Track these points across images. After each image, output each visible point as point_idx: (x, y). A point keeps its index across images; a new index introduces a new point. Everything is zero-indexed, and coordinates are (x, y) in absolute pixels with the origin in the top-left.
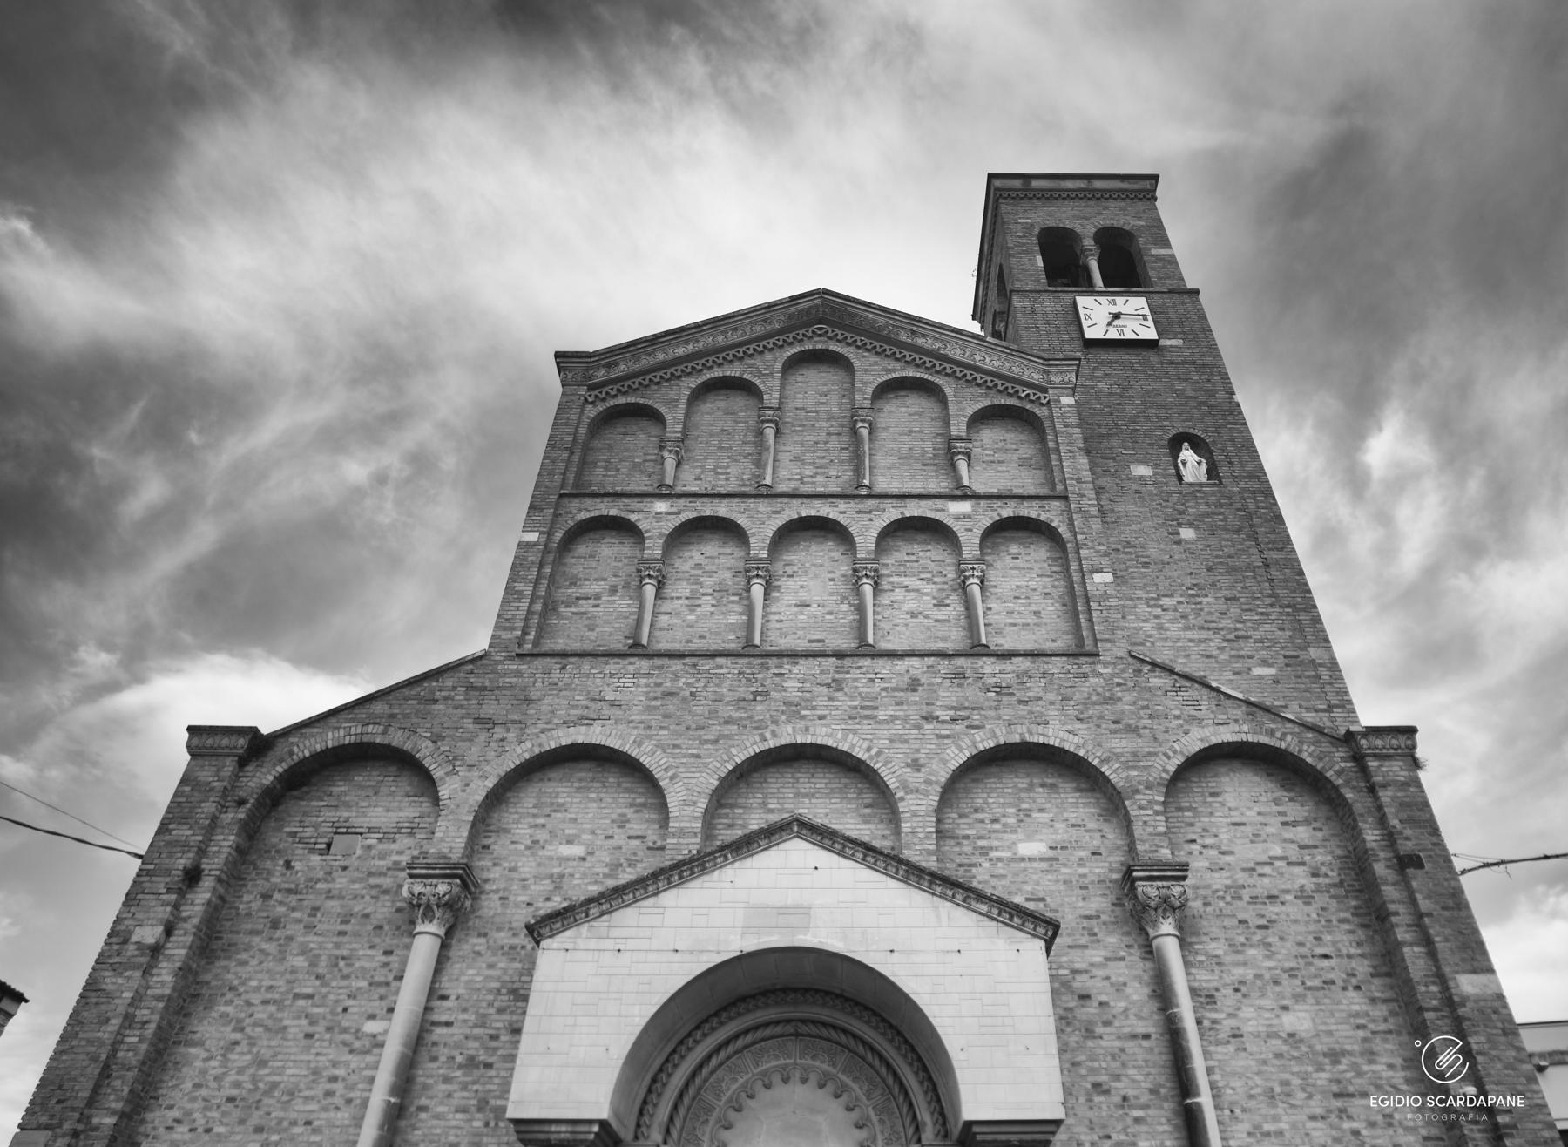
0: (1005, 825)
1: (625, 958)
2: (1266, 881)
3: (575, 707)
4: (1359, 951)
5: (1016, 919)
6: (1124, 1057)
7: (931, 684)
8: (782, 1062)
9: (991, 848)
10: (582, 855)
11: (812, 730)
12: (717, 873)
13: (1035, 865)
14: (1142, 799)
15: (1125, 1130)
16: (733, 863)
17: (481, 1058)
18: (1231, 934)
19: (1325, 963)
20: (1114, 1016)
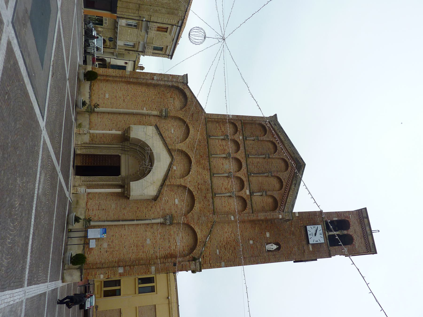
0: (180, 197)
2: (172, 241)
7: (205, 185)
10: (172, 132)
13: (174, 202)
14: (185, 219)
15: (132, 211)
20: (149, 212)
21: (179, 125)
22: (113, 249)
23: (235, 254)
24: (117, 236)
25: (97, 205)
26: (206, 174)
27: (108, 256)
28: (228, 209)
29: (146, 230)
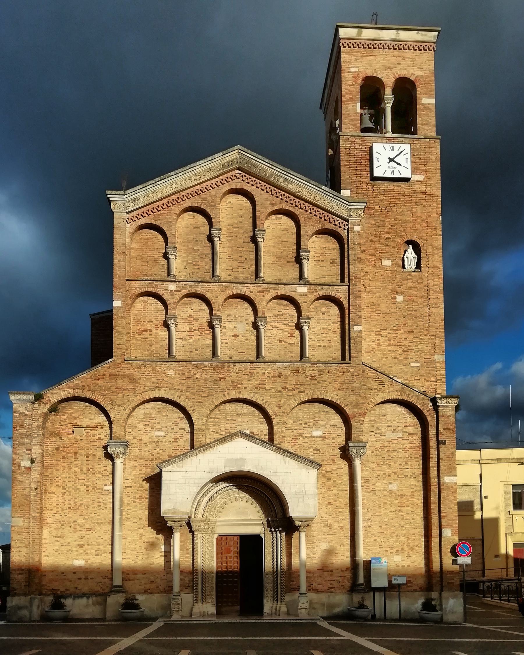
2: (394, 445)
4: (418, 467)
10: (164, 435)
13: (318, 439)
18: (379, 461)
19: (407, 470)
21: (144, 420)
22: (405, 545)
23: (421, 332)
24: (382, 540)
27: (417, 554)
28: (335, 335)
29: (373, 490)
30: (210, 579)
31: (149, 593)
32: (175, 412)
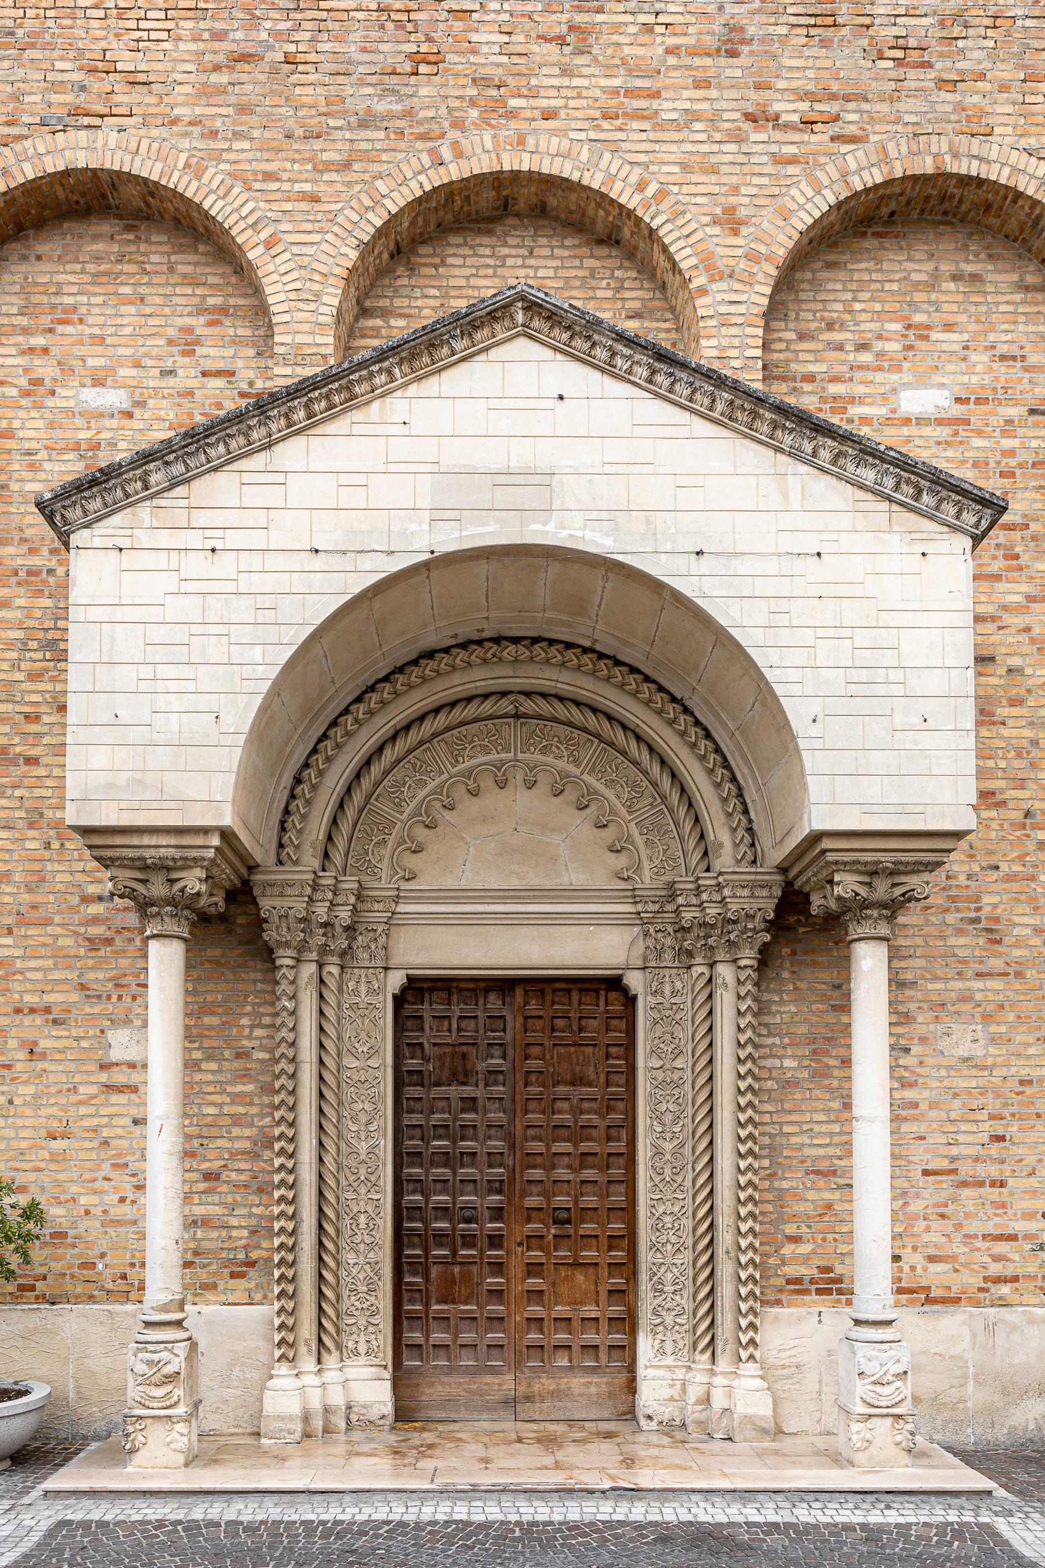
0: (879, 355)
1: (226, 563)
3: (57, 87)
5: (925, 498)
6: (1035, 753)
8: (494, 756)
9: (852, 400)
10: (126, 406)
11: (531, 141)
12: (376, 405)
13: (927, 431)
16: (405, 385)
17: (18, 749)
20: (1029, 691)
21: (24, 321)
25: (955, 1200)
26: (642, 18)
30: (362, 1219)
31: (42, 1298)
32: (185, 276)
